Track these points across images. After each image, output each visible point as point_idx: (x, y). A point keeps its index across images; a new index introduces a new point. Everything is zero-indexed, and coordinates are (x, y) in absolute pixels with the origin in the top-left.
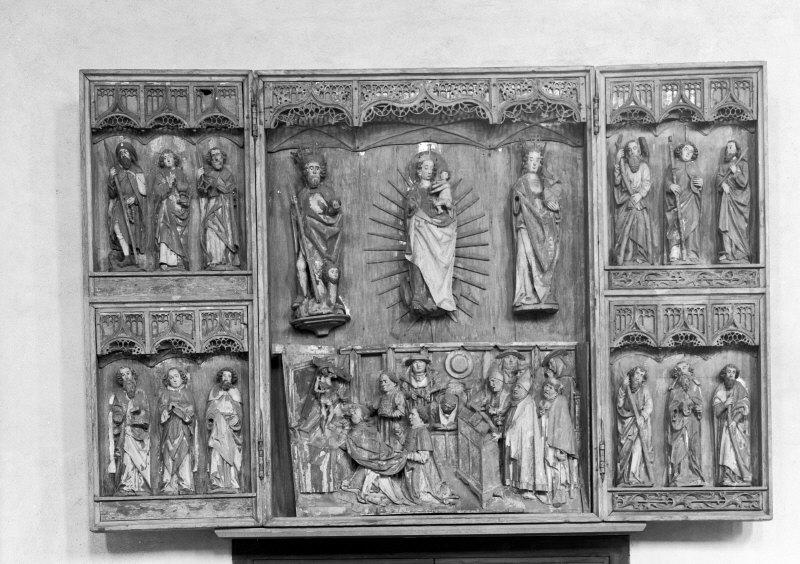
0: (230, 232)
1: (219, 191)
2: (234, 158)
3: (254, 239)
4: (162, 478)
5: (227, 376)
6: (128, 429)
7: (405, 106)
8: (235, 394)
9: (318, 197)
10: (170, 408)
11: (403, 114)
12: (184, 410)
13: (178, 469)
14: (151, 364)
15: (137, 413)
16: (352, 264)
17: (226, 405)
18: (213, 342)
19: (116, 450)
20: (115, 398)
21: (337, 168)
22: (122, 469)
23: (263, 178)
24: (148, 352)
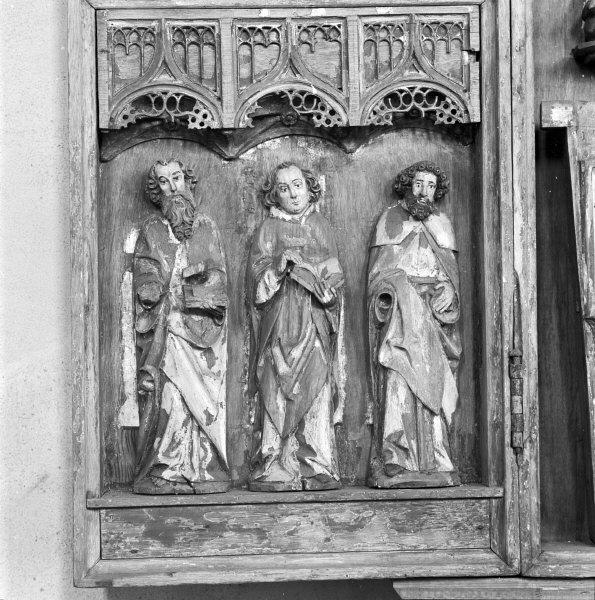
4: (259, 443)
5: (425, 184)
6: (175, 319)
8: (441, 227)
10: (283, 266)
12: (316, 270)
13: (301, 424)
14: (231, 152)
15: (200, 278)
17: (420, 254)
18: (393, 98)
19: (141, 373)
20: (142, 240)
22: (157, 422)
24: (228, 123)
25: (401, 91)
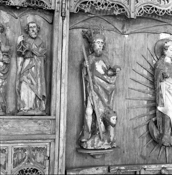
0: (39, 85)
1: (33, 54)
2: (46, 30)
3: (59, 93)
7: (163, 9)
9: (101, 62)
11: (161, 14)
16: (118, 108)
21: (110, 43)
23: (67, 47)
25: (24, 169)
